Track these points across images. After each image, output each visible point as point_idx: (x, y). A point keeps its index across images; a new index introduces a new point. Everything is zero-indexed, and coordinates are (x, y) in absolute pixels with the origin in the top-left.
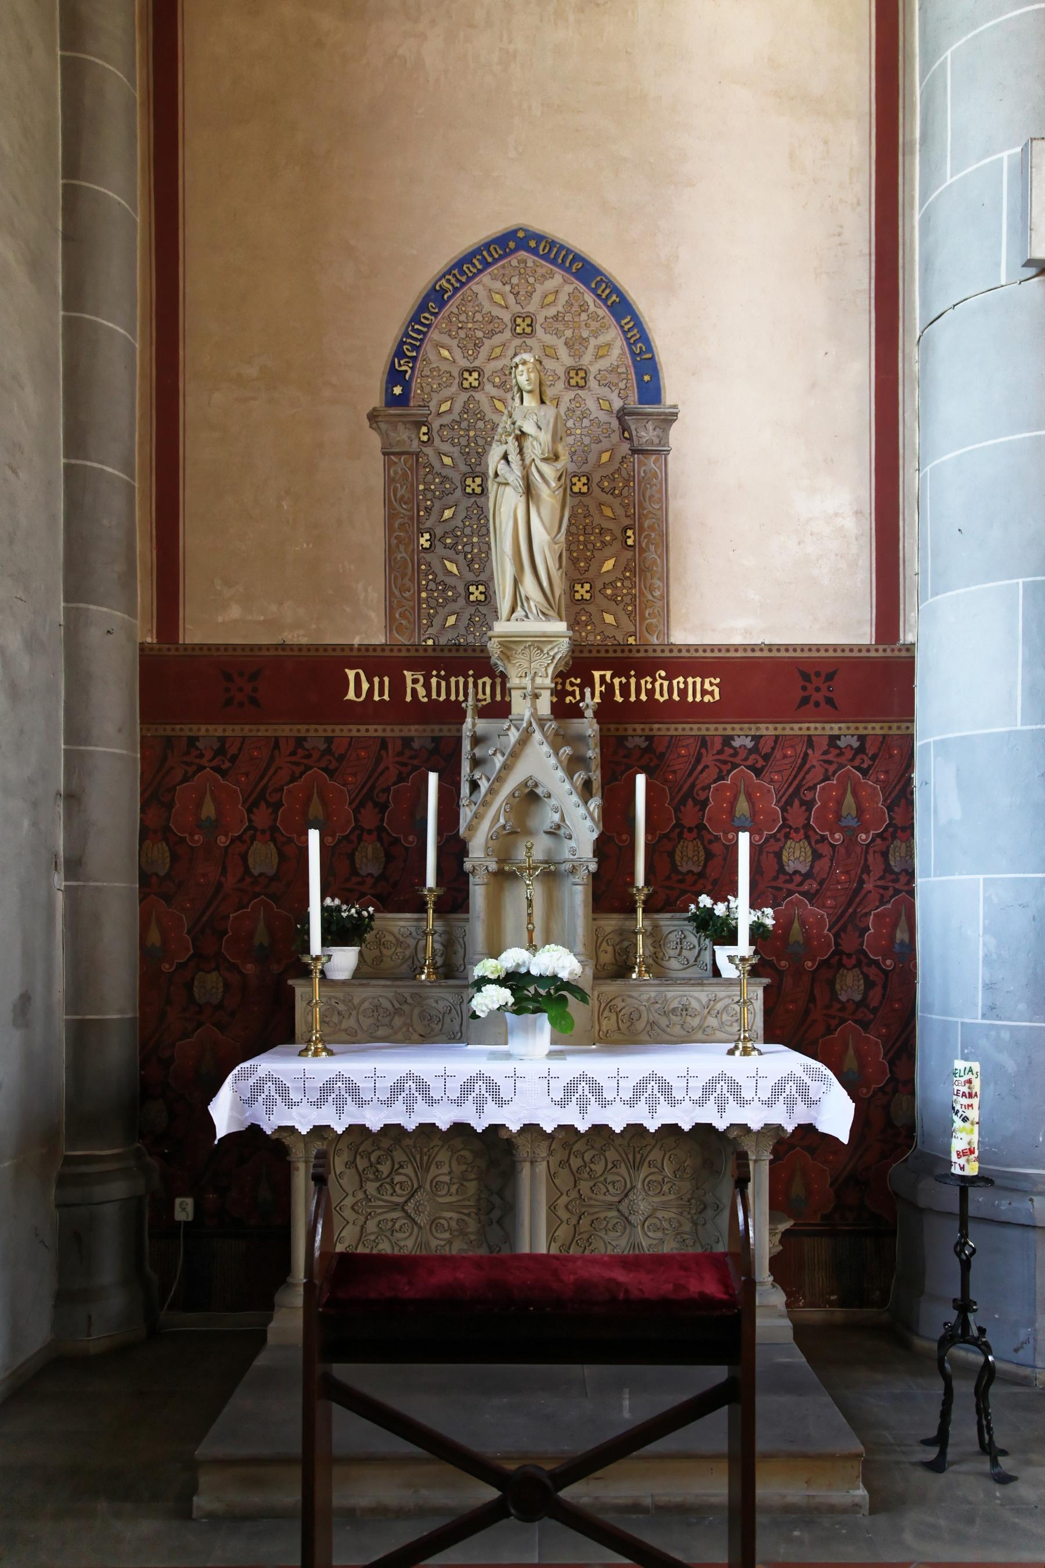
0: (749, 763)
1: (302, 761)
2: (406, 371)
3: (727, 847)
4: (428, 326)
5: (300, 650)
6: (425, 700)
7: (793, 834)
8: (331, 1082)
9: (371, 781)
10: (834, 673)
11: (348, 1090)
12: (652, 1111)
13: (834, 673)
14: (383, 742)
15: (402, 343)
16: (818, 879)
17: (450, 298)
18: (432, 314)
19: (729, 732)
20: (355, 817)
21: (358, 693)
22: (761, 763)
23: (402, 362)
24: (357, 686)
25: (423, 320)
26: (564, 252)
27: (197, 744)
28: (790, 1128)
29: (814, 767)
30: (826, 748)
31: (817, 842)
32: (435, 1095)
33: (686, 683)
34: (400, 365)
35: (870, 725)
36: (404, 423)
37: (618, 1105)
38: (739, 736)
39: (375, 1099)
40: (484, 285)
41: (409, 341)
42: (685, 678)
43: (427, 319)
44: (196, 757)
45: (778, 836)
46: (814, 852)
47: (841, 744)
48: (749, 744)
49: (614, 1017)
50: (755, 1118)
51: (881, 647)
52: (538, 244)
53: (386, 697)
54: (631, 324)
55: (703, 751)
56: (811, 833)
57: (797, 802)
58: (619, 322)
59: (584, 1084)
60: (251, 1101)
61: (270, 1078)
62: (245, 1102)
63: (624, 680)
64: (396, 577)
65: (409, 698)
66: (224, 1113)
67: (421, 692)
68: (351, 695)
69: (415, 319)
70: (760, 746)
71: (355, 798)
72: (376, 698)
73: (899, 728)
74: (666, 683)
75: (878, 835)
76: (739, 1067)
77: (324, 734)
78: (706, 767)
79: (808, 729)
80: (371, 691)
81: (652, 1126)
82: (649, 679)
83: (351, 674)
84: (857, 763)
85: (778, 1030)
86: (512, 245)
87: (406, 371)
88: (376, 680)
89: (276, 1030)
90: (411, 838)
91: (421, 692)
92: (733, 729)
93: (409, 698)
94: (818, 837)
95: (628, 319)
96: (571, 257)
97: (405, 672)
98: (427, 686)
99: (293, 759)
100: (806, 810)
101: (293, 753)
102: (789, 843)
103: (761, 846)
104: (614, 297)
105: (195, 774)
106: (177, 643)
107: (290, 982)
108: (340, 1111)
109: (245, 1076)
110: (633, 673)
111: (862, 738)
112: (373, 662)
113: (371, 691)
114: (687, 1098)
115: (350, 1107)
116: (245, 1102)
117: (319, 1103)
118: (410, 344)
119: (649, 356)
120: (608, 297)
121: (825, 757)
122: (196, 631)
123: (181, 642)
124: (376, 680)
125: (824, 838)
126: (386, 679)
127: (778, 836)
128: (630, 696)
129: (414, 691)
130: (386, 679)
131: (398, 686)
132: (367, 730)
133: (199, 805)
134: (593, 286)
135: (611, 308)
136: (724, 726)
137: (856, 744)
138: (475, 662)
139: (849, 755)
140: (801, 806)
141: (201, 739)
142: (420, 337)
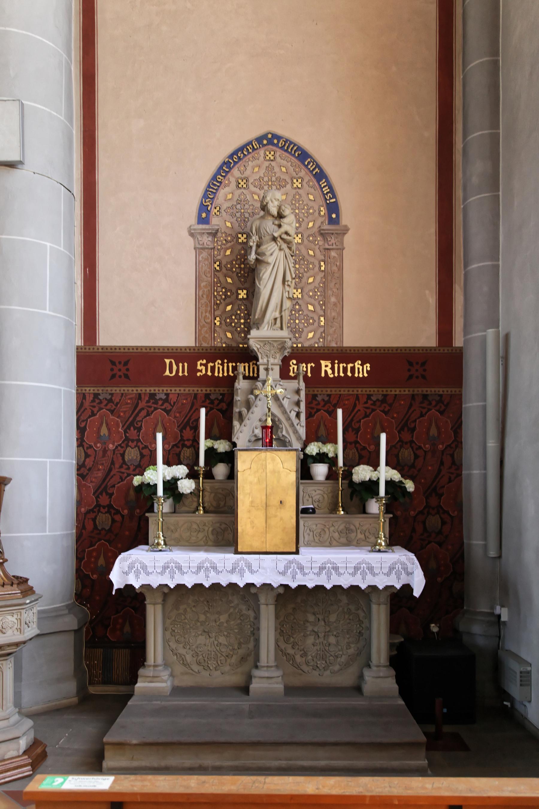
0: (325, 408)
1: (153, 405)
2: (209, 205)
3: (151, 451)
4: (221, 183)
5: (410, 350)
6: (332, 376)
7: (130, 443)
8: (203, 562)
9: (407, 416)
10: (128, 361)
11: (368, 568)
12: (364, 579)
13: (128, 361)
14: (357, 397)
15: (207, 191)
16: (88, 468)
17: (233, 166)
18: (222, 176)
19: (316, 393)
20: (181, 435)
21: (171, 372)
22: (443, 407)
23: (207, 201)
24: (173, 369)
25: (218, 180)
26: (292, 146)
27: (372, 397)
28: (398, 586)
29: (86, 409)
30: (204, 399)
31: (417, 449)
32: (150, 570)
33: (307, 367)
34: (205, 202)
35: (342, 389)
36: (208, 233)
37: (346, 576)
38: (320, 395)
39: (155, 571)
40: (277, 162)
41: (211, 190)
42: (307, 364)
43: (219, 178)
44: (371, 405)
45: (122, 445)
46: (86, 453)
47: (101, 397)
48: (164, 397)
49: (311, 533)
50: (381, 583)
51: (87, 347)
52: (278, 142)
53: (186, 374)
54: (325, 184)
55: (357, 402)
56: (413, 445)
57: (406, 429)
58: (318, 182)
59: (399, 564)
60: (127, 573)
61: (137, 560)
62: (124, 573)
63: (234, 364)
64: (202, 313)
65: (323, 375)
66: (118, 577)
67: (330, 372)
68: (167, 373)
69: (214, 178)
70: (331, 400)
71: (180, 425)
72: (180, 374)
73: (362, 391)
74: (296, 367)
75: (119, 445)
76: (374, 558)
77: (382, 393)
78: (86, 409)
79: (370, 391)
80: (178, 371)
81: (329, 586)
82: (304, 365)
83: (167, 361)
84: (109, 407)
85: (394, 541)
86: (265, 142)
87: (209, 205)
88: (181, 365)
89: (139, 537)
90: (98, 445)
91: (330, 372)
92: (318, 391)
93: (323, 375)
94: (88, 446)
95: (324, 180)
96: (295, 148)
97: (166, 360)
98: (333, 369)
99: (366, 405)
100: (137, 432)
101: (366, 403)
102: (128, 449)
103: (169, 451)
104: (317, 169)
105: (315, 413)
106: (96, 345)
107: (147, 515)
108: (172, 578)
109: (125, 560)
110: (336, 362)
111: (167, 395)
112: (179, 355)
113: (178, 371)
114: (346, 572)
115: (143, 575)
116: (124, 573)
117: (162, 573)
118: (211, 191)
119: (334, 200)
120: (314, 170)
121: (92, 404)
122: (107, 338)
123: (97, 344)
124: (181, 365)
125: (420, 447)
126: (186, 364)
127: (122, 445)
128: (355, 373)
129: (326, 372)
130: (186, 364)
131: (193, 369)
132: (353, 391)
133: (429, 429)
134: (306, 163)
135: (315, 176)
136: (317, 389)
137: (164, 397)
138: (250, 357)
139: (105, 402)
140: (134, 430)
141: (319, 395)
142: (216, 188)
